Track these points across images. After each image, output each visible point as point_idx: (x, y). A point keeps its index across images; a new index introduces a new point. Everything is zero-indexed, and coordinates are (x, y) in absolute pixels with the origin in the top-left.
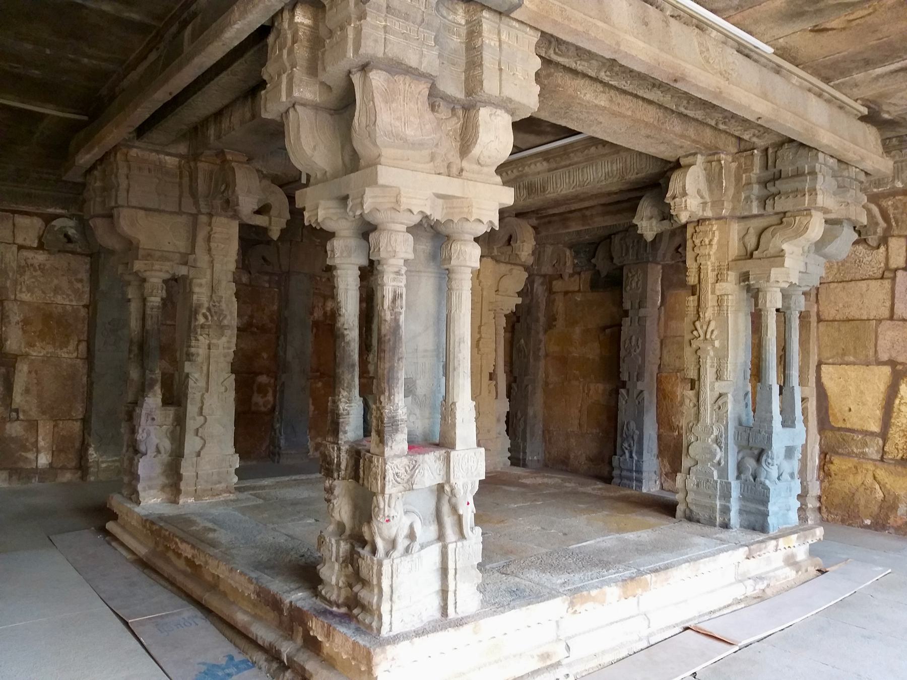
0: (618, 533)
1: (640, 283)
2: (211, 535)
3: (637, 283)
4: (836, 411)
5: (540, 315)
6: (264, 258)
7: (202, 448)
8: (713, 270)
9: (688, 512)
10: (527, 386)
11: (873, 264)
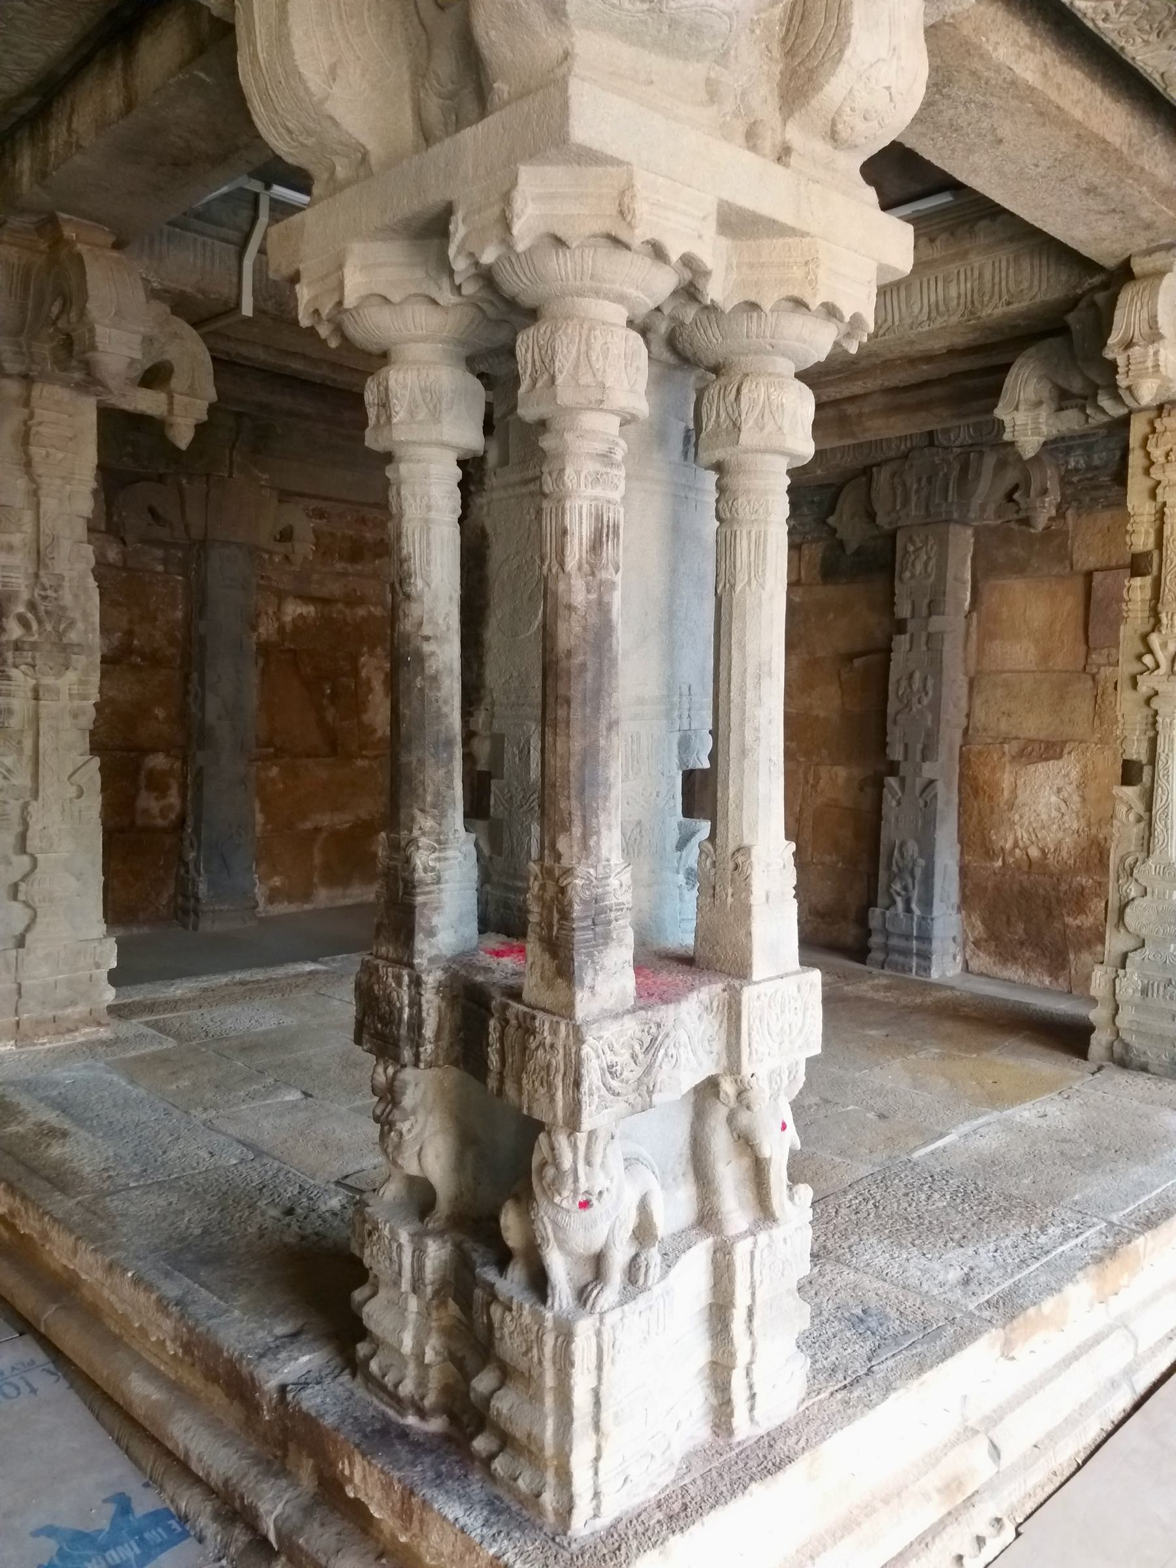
0: (993, 1107)
1: (932, 563)
2: (56, 1151)
3: (926, 564)
6: (152, 511)
7: (28, 928)
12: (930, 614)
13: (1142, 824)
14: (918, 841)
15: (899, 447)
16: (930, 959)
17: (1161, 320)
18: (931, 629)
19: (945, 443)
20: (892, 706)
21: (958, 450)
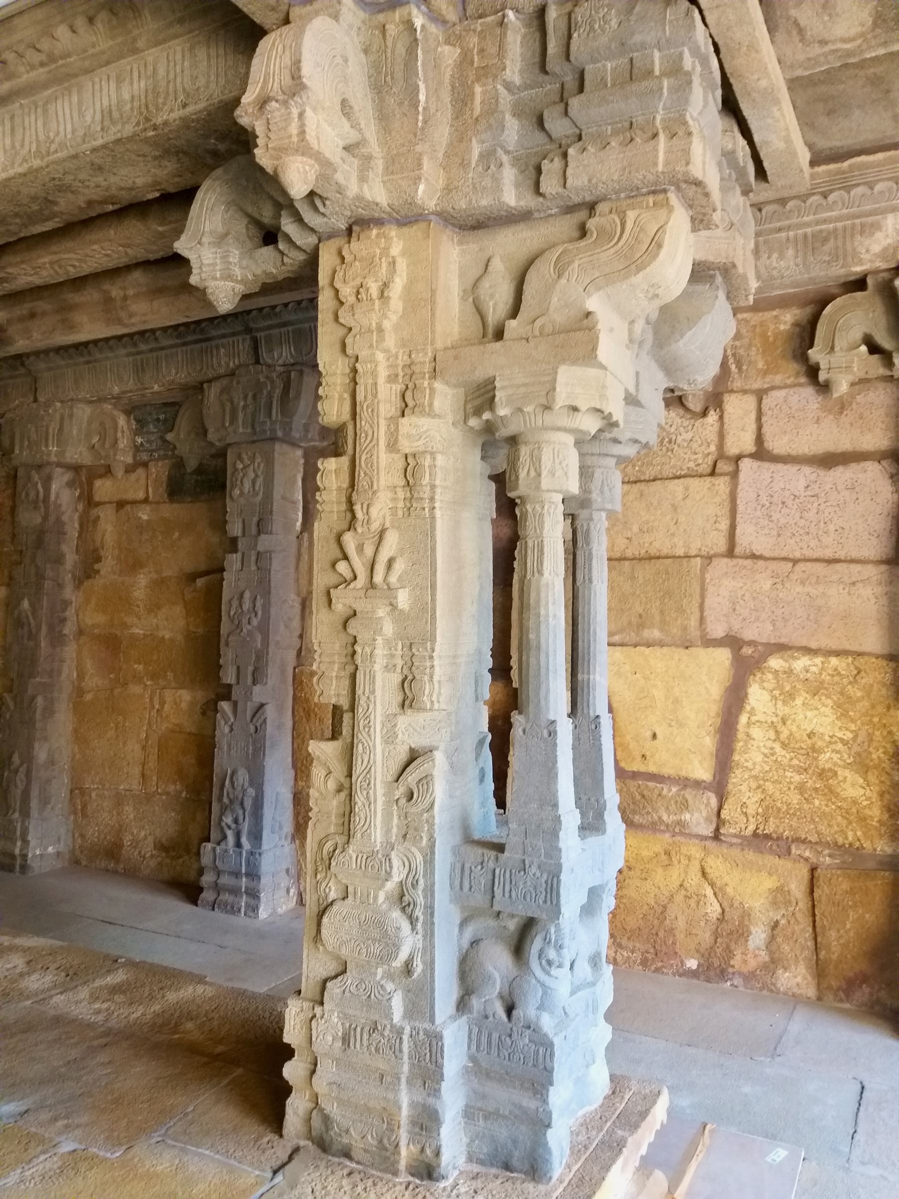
1: (260, 481)
3: (254, 482)
4: (628, 737)
5: (65, 548)
8: (392, 379)
9: (316, 1122)
10: (33, 698)
11: (695, 445)
12: (259, 533)
13: (343, 795)
14: (248, 769)
15: (228, 364)
16: (259, 898)
17: (306, 70)
18: (260, 548)
19: (270, 361)
20: (225, 628)
21: (282, 369)
